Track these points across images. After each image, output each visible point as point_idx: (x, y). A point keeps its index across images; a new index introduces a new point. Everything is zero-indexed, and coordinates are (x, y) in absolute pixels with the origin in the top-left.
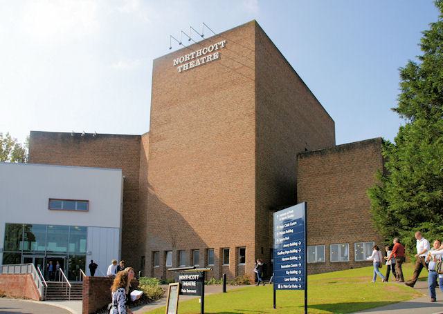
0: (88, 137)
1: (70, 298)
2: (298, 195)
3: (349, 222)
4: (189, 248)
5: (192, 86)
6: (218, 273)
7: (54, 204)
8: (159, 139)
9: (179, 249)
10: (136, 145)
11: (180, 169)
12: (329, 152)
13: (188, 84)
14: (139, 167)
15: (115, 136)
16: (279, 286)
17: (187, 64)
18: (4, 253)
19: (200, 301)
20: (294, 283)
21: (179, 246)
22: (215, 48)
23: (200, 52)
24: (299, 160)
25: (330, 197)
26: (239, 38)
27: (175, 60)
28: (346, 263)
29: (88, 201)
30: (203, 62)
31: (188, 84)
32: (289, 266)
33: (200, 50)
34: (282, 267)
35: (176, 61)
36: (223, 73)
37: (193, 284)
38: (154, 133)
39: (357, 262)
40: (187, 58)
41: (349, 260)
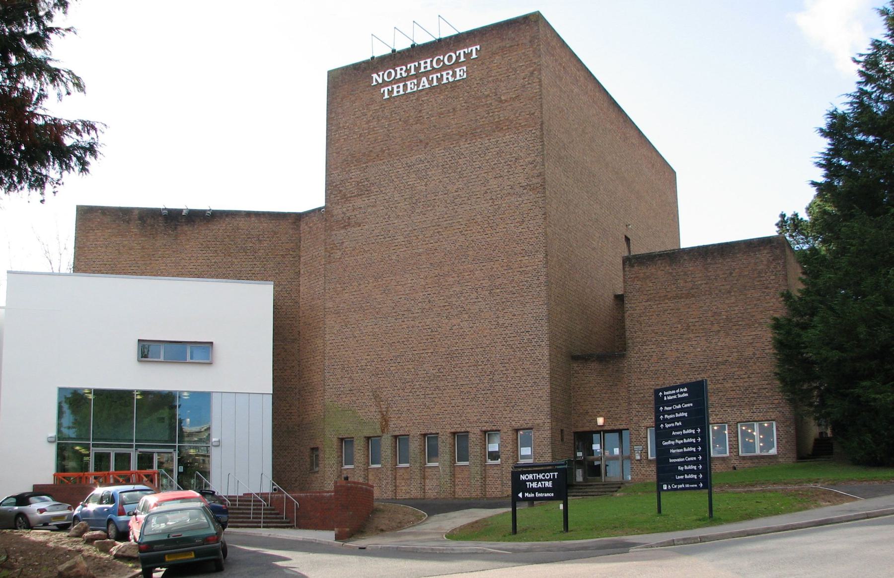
0: (196, 217)
1: (262, 525)
2: (627, 333)
3: (728, 385)
4: (415, 432)
5: (414, 127)
6: (478, 477)
7: (147, 351)
8: (346, 224)
9: (397, 433)
10: (291, 232)
11: (394, 283)
12: (686, 257)
13: (405, 122)
14: (298, 274)
15: (249, 214)
16: (665, 487)
17: (401, 85)
18: (58, 444)
19: (561, 507)
20: (691, 481)
21: (397, 426)
22: (458, 57)
23: (426, 64)
24: (627, 269)
25: (689, 339)
26: (508, 43)
27: (375, 76)
28: (723, 459)
29: (212, 343)
30: (435, 83)
31: (405, 122)
32: (683, 460)
33: (429, 61)
34: (671, 461)
35: (377, 78)
36: (478, 107)
37: (549, 484)
38: (335, 212)
39: (744, 458)
40: (401, 71)
41: (728, 454)
